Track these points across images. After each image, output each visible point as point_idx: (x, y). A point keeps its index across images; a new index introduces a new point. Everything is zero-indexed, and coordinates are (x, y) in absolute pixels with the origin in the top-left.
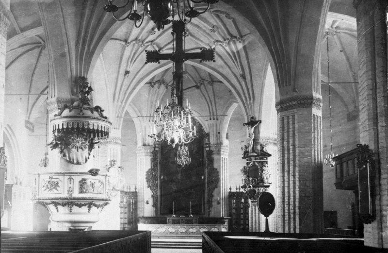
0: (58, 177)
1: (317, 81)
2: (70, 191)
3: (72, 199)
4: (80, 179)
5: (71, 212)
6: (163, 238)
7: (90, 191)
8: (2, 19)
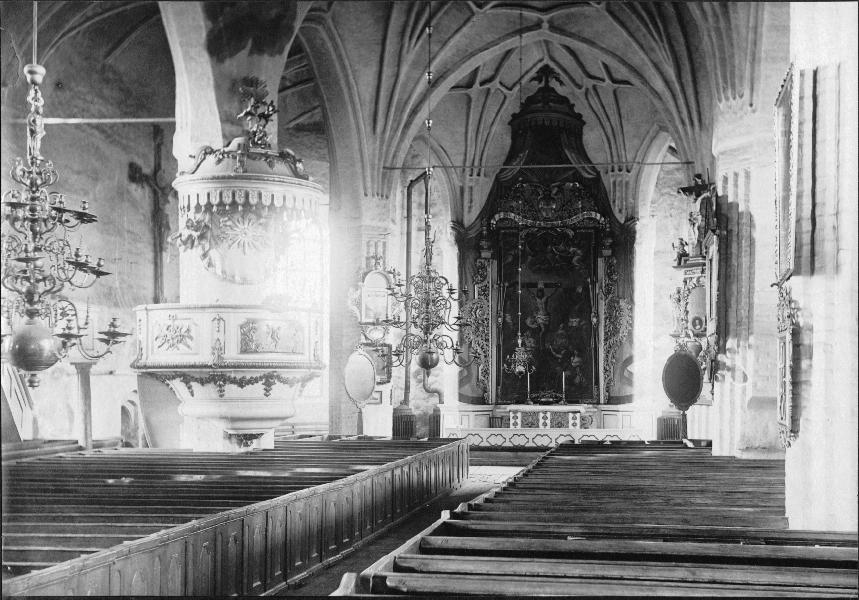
0: (188, 316)
1: (358, 93)
2: (219, 349)
3: (221, 367)
4: (242, 321)
5: (221, 396)
6: (496, 528)
7: (267, 349)
8: (33, 109)
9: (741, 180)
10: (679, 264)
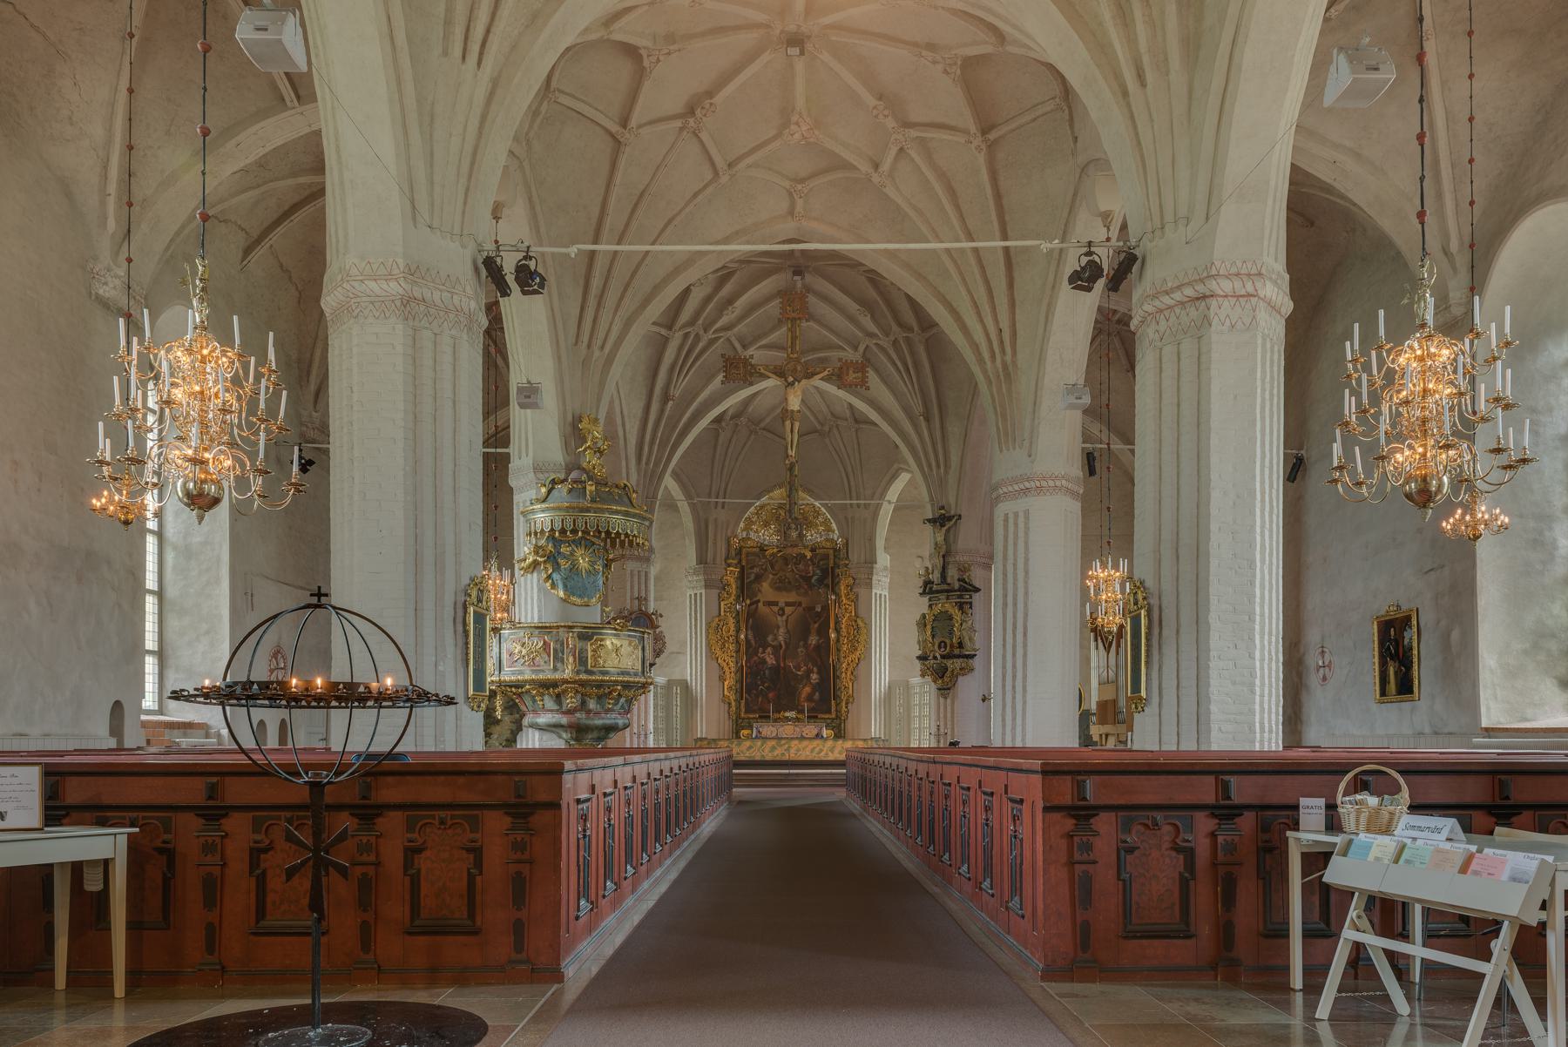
9: (1021, 520)
10: (924, 590)
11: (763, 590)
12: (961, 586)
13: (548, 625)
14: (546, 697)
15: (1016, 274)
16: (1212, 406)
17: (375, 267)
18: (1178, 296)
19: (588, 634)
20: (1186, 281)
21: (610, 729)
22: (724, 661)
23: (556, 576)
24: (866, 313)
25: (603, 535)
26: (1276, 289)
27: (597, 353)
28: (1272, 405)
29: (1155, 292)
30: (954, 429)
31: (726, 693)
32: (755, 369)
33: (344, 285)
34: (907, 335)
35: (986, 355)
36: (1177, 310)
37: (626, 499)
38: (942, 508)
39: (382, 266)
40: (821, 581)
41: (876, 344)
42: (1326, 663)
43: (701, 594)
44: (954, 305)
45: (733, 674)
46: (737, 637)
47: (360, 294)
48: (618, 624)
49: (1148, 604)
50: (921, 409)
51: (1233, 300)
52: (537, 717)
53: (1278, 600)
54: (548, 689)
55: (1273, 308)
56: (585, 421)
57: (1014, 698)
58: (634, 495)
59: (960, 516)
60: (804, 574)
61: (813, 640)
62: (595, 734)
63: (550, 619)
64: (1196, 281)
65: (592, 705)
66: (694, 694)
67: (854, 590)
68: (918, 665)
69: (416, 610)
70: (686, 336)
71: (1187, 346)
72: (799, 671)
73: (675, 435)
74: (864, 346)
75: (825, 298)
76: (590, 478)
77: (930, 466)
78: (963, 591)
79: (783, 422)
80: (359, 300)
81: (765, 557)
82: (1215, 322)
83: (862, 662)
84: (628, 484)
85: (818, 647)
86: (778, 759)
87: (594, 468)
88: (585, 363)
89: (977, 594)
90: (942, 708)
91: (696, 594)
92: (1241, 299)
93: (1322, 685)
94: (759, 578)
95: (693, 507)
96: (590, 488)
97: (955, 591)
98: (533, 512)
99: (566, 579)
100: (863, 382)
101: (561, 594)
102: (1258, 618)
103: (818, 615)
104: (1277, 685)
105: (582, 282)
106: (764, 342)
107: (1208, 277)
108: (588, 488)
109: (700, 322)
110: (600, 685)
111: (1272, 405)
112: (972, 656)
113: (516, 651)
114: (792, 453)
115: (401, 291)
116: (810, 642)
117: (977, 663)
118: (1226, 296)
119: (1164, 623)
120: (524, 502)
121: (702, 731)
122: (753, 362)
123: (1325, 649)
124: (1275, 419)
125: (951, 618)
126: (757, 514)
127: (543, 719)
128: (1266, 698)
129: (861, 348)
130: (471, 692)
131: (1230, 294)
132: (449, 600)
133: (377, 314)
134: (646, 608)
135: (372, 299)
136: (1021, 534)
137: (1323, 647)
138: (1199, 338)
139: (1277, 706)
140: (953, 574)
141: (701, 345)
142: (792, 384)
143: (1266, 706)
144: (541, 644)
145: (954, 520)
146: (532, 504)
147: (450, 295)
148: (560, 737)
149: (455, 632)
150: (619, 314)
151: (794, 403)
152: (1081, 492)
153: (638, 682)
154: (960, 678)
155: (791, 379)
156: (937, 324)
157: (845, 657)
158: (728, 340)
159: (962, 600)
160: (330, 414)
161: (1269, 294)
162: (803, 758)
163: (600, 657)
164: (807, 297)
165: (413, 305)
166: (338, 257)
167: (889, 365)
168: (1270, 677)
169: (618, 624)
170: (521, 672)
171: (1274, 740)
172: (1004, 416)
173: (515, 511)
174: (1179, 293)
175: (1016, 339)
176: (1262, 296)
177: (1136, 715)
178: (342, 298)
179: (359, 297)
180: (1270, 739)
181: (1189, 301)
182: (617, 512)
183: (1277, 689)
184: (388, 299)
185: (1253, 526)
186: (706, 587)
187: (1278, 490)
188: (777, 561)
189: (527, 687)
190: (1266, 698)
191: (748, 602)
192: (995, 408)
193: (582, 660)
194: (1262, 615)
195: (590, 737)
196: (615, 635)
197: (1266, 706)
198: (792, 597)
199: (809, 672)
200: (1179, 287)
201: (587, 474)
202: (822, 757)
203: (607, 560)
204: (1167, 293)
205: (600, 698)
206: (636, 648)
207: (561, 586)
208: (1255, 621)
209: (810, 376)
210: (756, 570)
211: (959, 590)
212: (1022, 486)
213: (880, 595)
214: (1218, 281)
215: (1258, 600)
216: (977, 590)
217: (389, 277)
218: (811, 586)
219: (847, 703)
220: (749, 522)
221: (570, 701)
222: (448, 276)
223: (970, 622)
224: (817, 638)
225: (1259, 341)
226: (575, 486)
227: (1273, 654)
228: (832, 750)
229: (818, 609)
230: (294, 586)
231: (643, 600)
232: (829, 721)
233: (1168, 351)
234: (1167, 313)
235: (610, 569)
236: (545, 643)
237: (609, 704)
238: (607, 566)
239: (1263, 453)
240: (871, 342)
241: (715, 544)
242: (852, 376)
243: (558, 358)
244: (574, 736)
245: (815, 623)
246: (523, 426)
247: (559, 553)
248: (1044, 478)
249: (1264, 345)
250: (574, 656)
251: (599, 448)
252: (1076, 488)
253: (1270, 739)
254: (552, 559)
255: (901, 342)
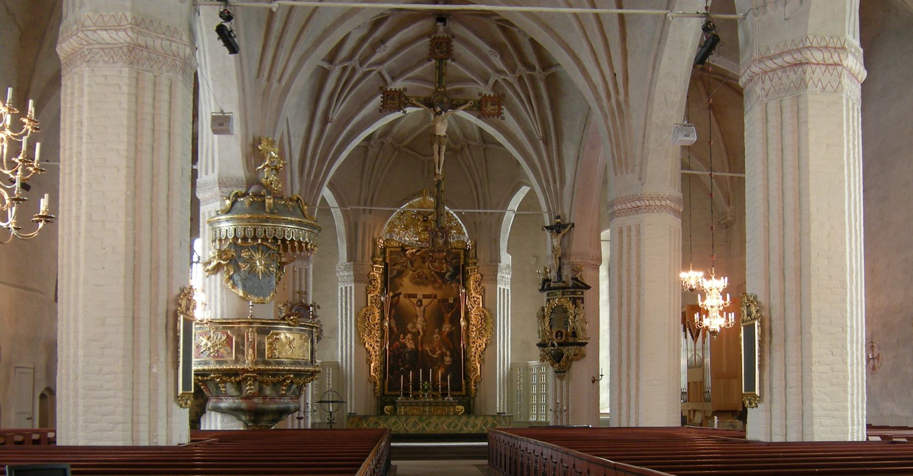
9: (633, 233)
11: (403, 284)
12: (574, 283)
13: (230, 321)
14: (228, 385)
15: (628, 30)
16: (810, 153)
17: (106, 19)
18: (779, 61)
19: (265, 329)
20: (786, 50)
21: (282, 413)
22: (371, 345)
23: (236, 277)
24: (496, 54)
25: (279, 242)
26: (855, 61)
27: (275, 85)
28: (854, 153)
29: (760, 57)
30: (569, 152)
31: (372, 374)
32: (408, 100)
33: (79, 34)
34: (530, 73)
35: (603, 95)
36: (779, 73)
37: (300, 212)
38: (558, 217)
39: (112, 18)
40: (453, 277)
41: (503, 79)
42: (876, 356)
43: (351, 287)
44: (577, 52)
45: (378, 357)
46: (382, 325)
47: (92, 42)
48: (291, 320)
49: (761, 316)
50: (541, 134)
51: (823, 68)
52: (219, 402)
53: (862, 314)
54: (230, 377)
55: (853, 75)
56: (264, 143)
57: (628, 384)
58: (306, 207)
59: (573, 225)
60: (438, 271)
61: (446, 328)
62: (270, 417)
63: (230, 315)
64: (793, 50)
65: (268, 391)
66: (344, 374)
67: (481, 285)
68: (538, 351)
69: (133, 318)
70: (344, 69)
71: (787, 102)
72: (435, 354)
73: (332, 152)
74: (494, 80)
75: (464, 41)
76: (269, 193)
77: (547, 181)
78: (576, 288)
79: (432, 145)
80: (91, 47)
81: (405, 255)
82: (810, 84)
83: (488, 346)
84: (301, 198)
85: (450, 334)
86: (420, 432)
87: (272, 184)
88: (265, 94)
89: (588, 291)
90: (558, 389)
91: (346, 288)
92: (829, 67)
93: (872, 374)
94: (400, 274)
95: (345, 214)
96: (269, 201)
97: (570, 288)
98: (219, 221)
99: (245, 280)
100: (499, 114)
101: (241, 293)
102: (849, 329)
103: (451, 306)
104: (862, 384)
105: (264, 26)
106: (410, 75)
107: (804, 48)
108: (267, 201)
109: (357, 57)
110: (275, 373)
111: (854, 153)
112: (584, 344)
113: (203, 344)
114: (439, 171)
115: (128, 40)
116: (444, 330)
117: (588, 349)
118: (818, 64)
119: (773, 332)
120: (209, 212)
121: (351, 407)
122: (407, 94)
123: (874, 345)
124: (857, 164)
125: (566, 311)
126: (399, 218)
127: (224, 404)
128: (855, 396)
129: (491, 82)
130: (180, 391)
131: (821, 62)
132: (162, 310)
133: (106, 59)
134: (306, 301)
135: (103, 46)
136: (634, 245)
137: (872, 342)
138: (797, 96)
139: (863, 402)
140: (567, 273)
141: (357, 76)
142: (440, 113)
143: (855, 403)
144: (224, 337)
145: (568, 228)
146: (218, 215)
147: (169, 42)
148: (240, 419)
149: (167, 337)
150: (295, 52)
151: (442, 129)
152: (681, 210)
153: (308, 371)
154: (574, 364)
155: (438, 109)
156: (559, 64)
157: (474, 343)
158: (380, 73)
159: (576, 296)
160: (62, 144)
161: (850, 64)
162: (440, 432)
163: (276, 349)
164: (452, 41)
165: (137, 51)
166: (74, 10)
167: (515, 97)
168: (857, 379)
169: (291, 320)
170: (206, 363)
171: (860, 432)
172: (618, 145)
173: (201, 220)
174: (781, 59)
175: (628, 83)
176: (845, 65)
177: (749, 410)
178: (77, 45)
179: (91, 44)
180: (858, 431)
181: (789, 66)
182: (292, 222)
183: (862, 388)
184: (117, 46)
185: (844, 253)
186: (356, 281)
187: (860, 223)
188: (416, 259)
189: (212, 376)
190: (855, 396)
191: (391, 294)
192: (610, 139)
193: (260, 352)
194: (852, 327)
195: (265, 419)
196: (288, 329)
197: (855, 403)
198: (429, 290)
199: (443, 355)
200: (780, 55)
201: (266, 189)
202: (457, 430)
203: (279, 263)
204: (771, 58)
205: (275, 385)
206: (306, 341)
207: (240, 286)
208: (847, 333)
209: (455, 107)
210: (398, 267)
211: (573, 287)
212: (634, 205)
213: (504, 289)
214: (812, 51)
215: (848, 314)
216: (588, 287)
217: (118, 28)
218: (445, 282)
219: (475, 382)
220: (392, 226)
221: (249, 389)
222: (168, 26)
223: (582, 315)
224: (450, 326)
225: (844, 102)
226: (255, 199)
227: (859, 359)
228: (466, 425)
229: (451, 301)
230: (8, 284)
231: (303, 293)
232: (460, 398)
233: (773, 105)
234: (770, 74)
235: (283, 270)
236: (228, 336)
237: (283, 390)
238: (280, 268)
239: (850, 192)
240: (500, 78)
241: (363, 244)
242: (490, 108)
243: (243, 90)
244: (252, 418)
245: (448, 313)
246: (210, 147)
247: (240, 257)
248: (652, 199)
249: (847, 105)
250: (253, 348)
251: (276, 166)
252: (677, 207)
253: (858, 431)
254: (233, 262)
255: (525, 79)
